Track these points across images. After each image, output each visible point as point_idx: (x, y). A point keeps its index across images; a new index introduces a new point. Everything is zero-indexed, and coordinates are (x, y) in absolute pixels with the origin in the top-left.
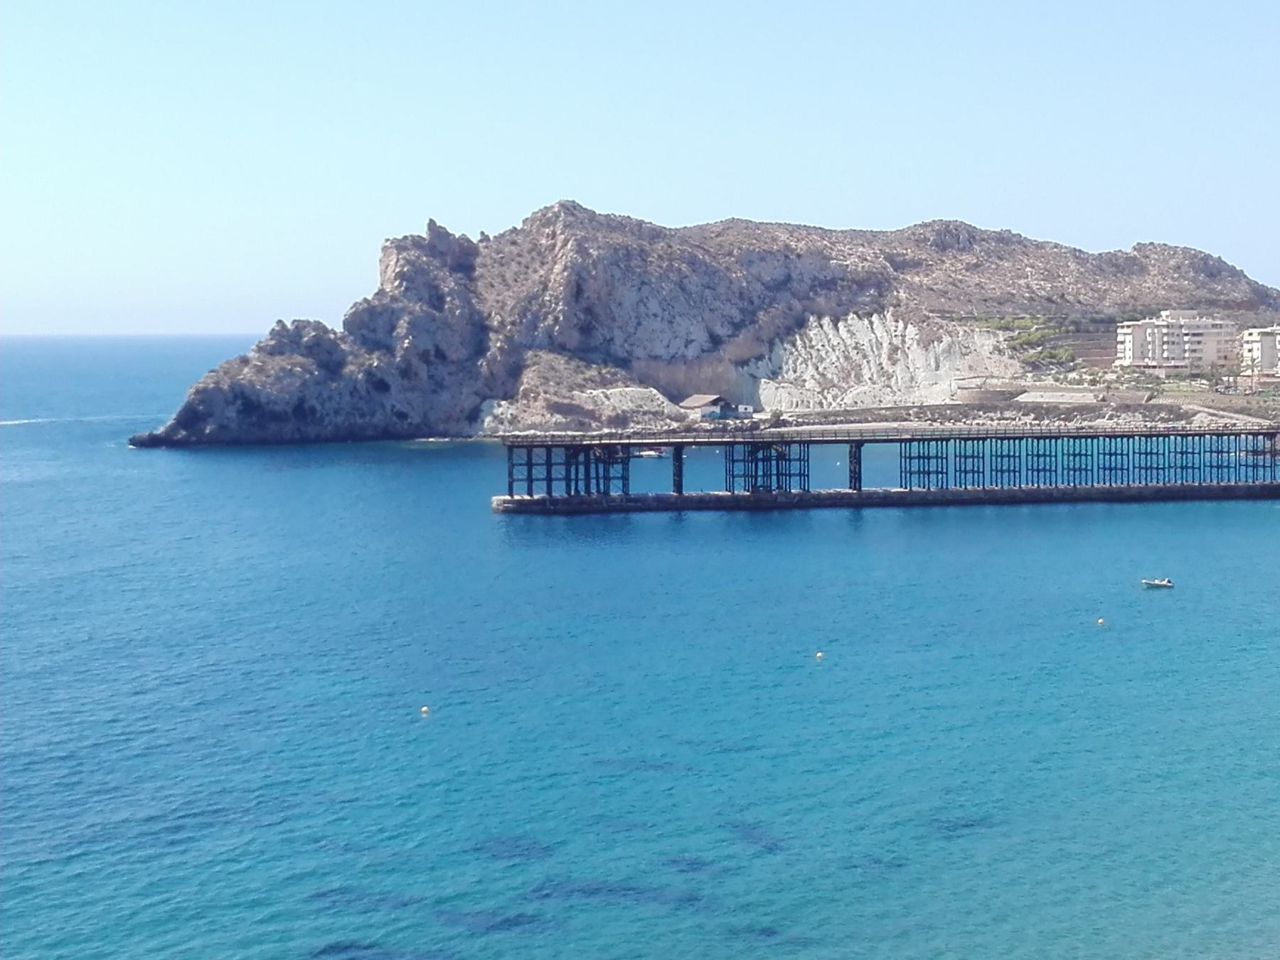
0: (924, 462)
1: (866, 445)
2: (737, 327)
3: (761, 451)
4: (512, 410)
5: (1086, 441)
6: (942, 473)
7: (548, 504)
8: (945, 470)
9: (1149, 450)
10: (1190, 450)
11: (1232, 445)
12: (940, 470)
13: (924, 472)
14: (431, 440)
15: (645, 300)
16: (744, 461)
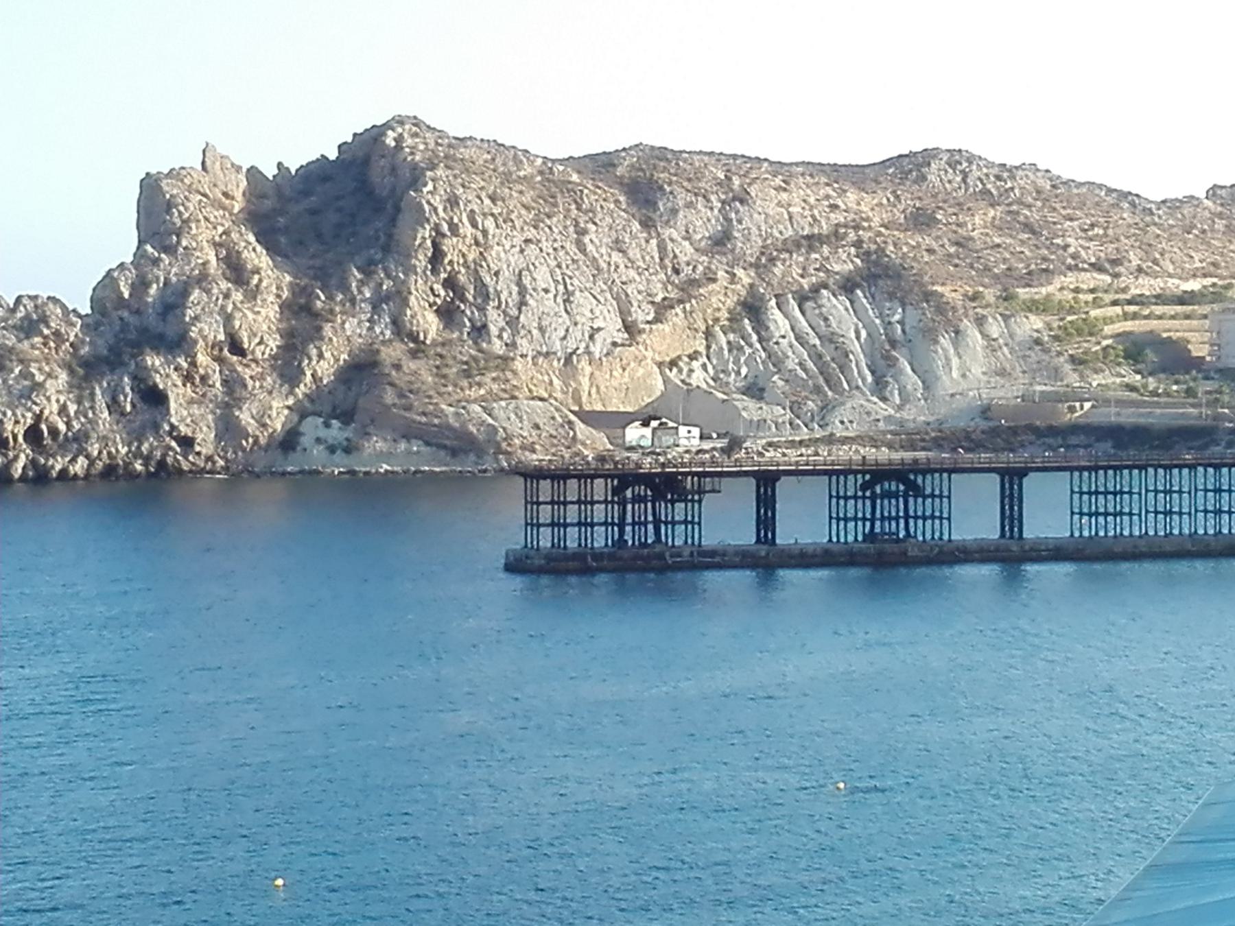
0: (613, 507)
1: (1032, 475)
2: (662, 310)
3: (630, 489)
4: (348, 433)
5: (941, 475)
6: (692, 522)
7: (589, 559)
8: (696, 519)
9: (1093, 489)
10: (1126, 489)
11: (1185, 483)
12: (689, 518)
13: (559, 525)
14: (427, 468)
15: (531, 267)
16: (606, 502)
